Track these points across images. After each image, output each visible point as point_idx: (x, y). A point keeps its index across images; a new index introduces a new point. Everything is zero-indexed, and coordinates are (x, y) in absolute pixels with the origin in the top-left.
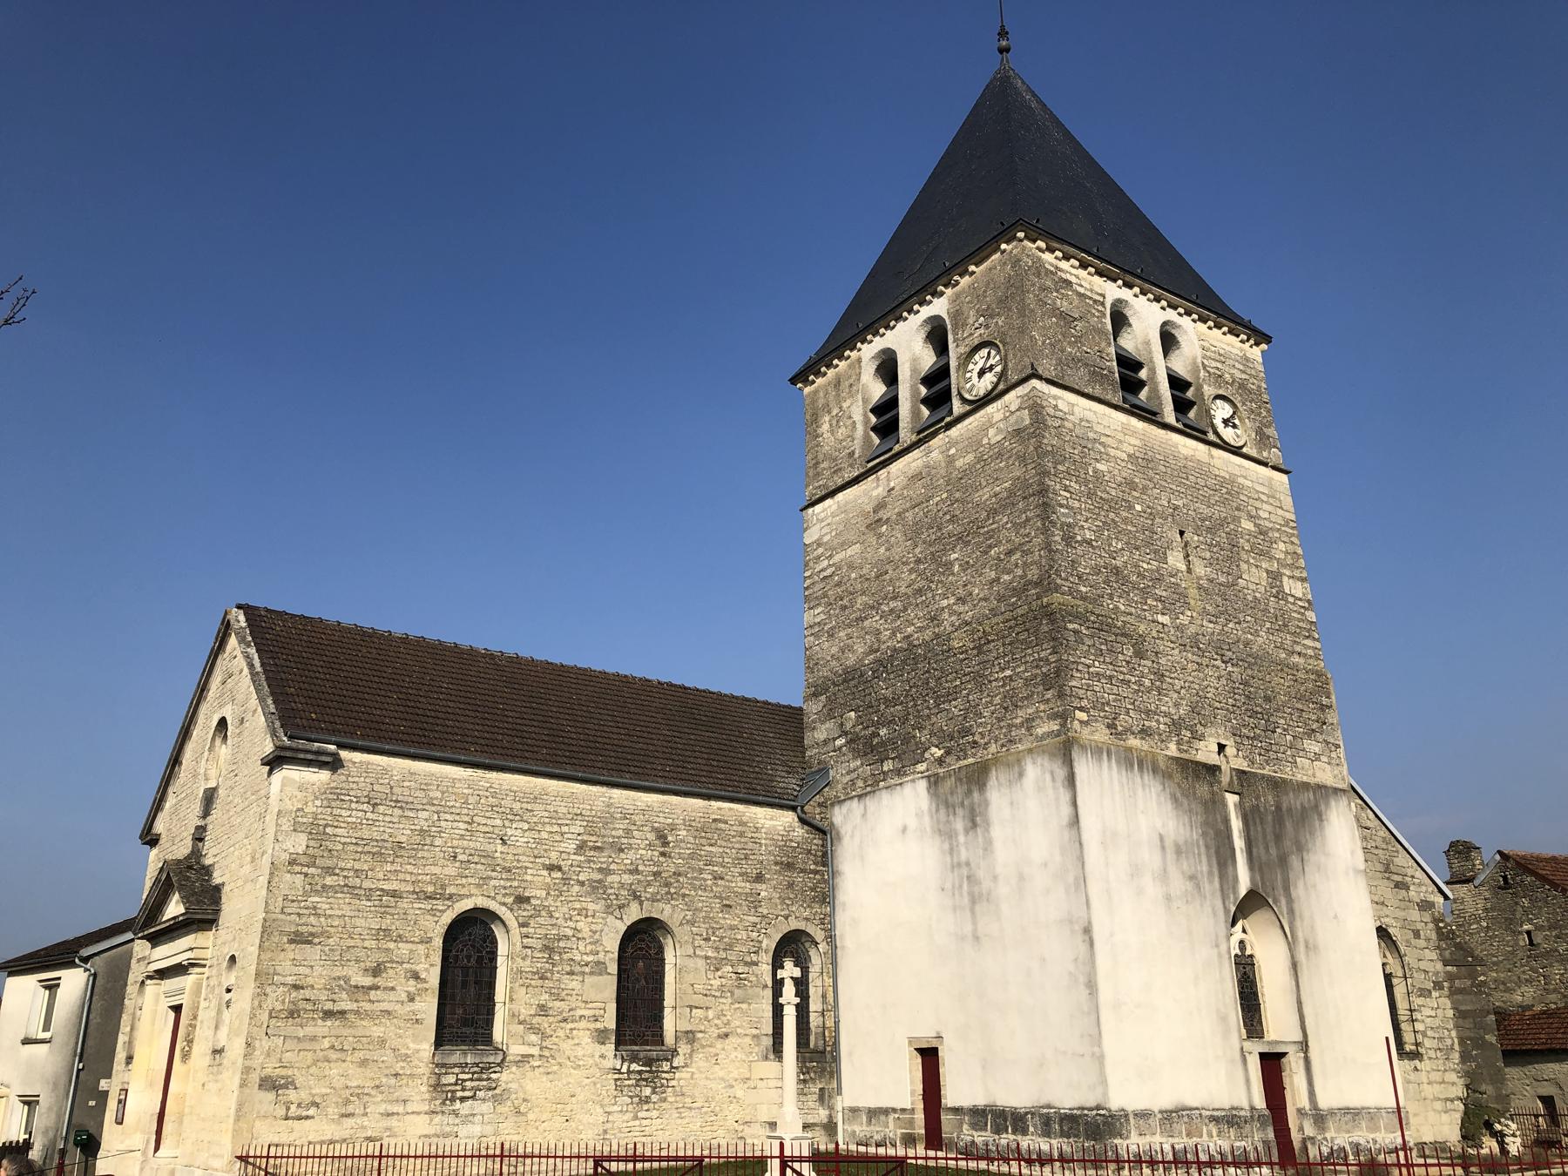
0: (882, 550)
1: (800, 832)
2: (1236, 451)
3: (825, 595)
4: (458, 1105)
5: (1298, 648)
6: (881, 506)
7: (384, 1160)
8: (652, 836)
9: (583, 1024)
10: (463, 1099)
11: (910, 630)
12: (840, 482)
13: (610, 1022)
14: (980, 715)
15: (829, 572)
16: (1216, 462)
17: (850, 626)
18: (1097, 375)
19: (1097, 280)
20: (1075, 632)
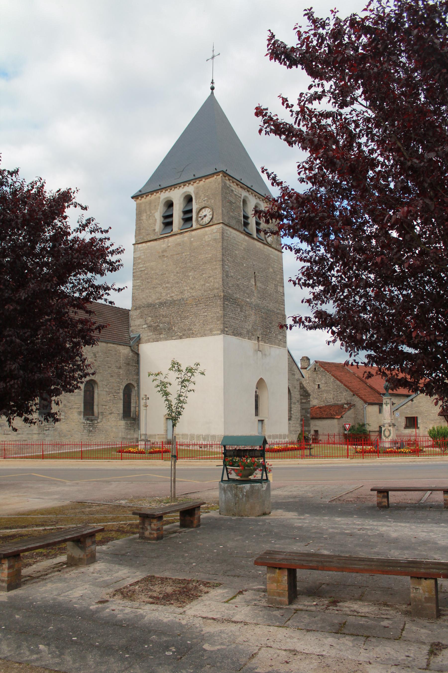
0: (164, 266)
1: (131, 354)
2: (270, 246)
3: (141, 277)
4: (45, 432)
5: (280, 308)
6: (164, 251)
7: (44, 446)
8: (92, 355)
9: (75, 410)
10: (46, 430)
11: (173, 294)
12: (149, 239)
13: (82, 410)
14: (195, 325)
15: (143, 269)
16: (265, 250)
17: (150, 289)
18: (238, 221)
19: (240, 190)
20: (227, 304)
